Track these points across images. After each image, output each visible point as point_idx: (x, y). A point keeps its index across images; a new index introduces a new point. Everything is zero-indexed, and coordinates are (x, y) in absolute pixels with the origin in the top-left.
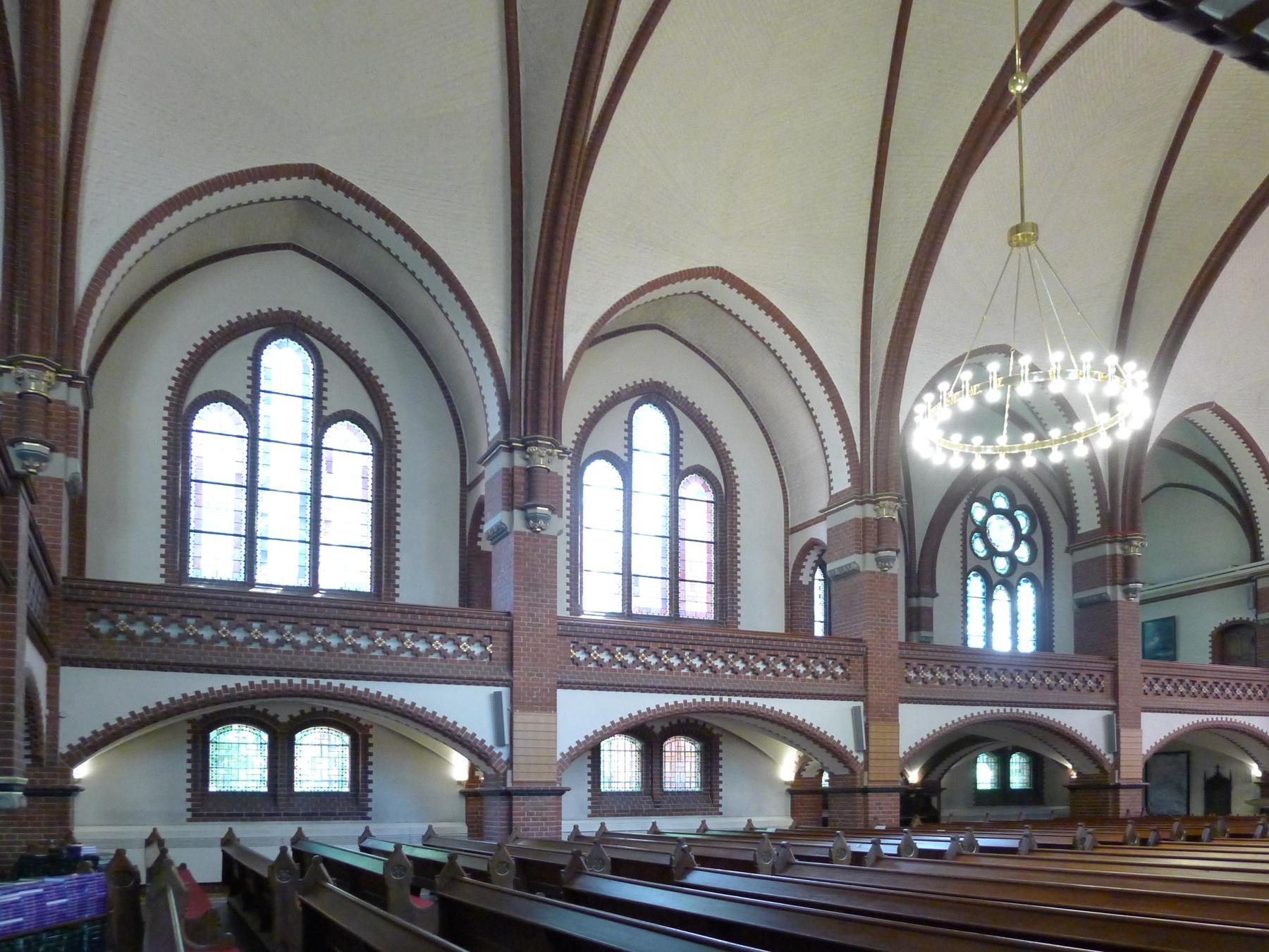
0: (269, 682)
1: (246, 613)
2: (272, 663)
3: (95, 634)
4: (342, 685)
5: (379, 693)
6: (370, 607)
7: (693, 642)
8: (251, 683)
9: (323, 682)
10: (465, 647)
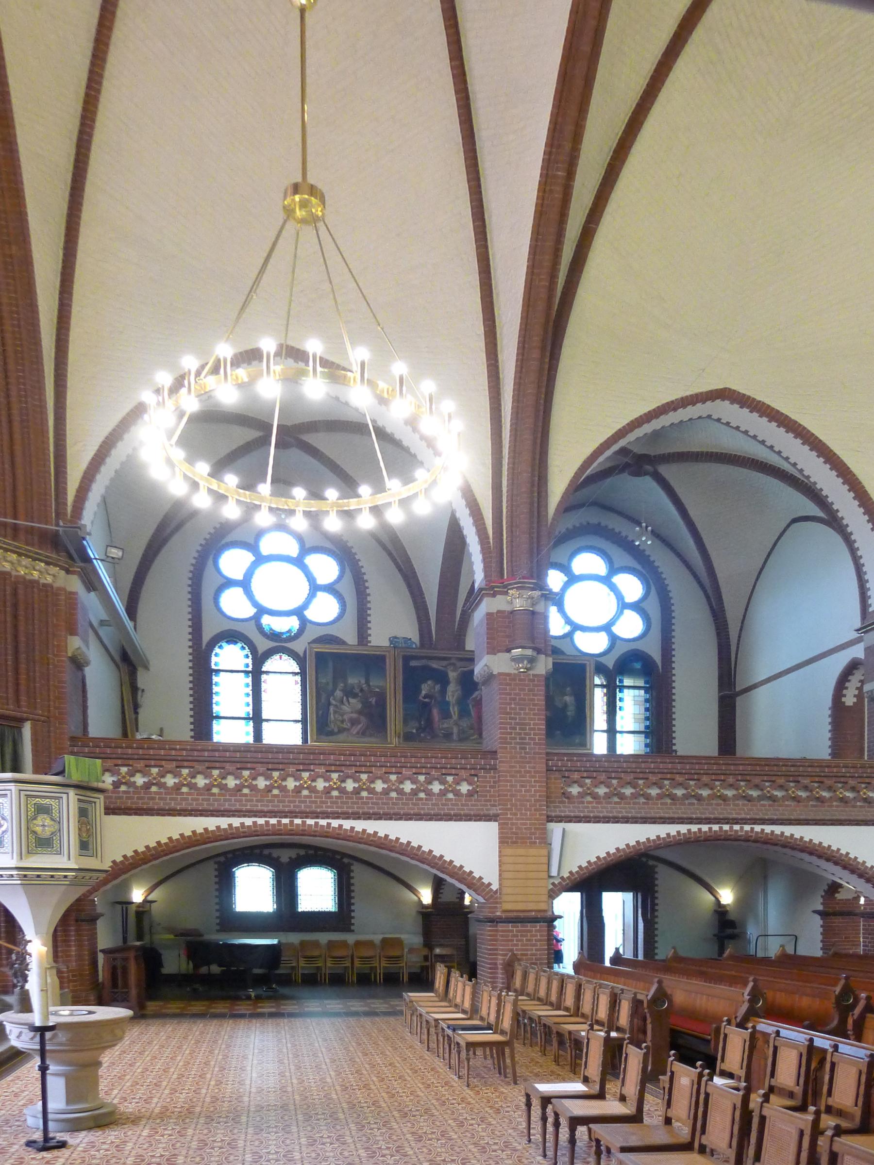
0: (693, 830)
1: (685, 774)
2: (173, 805)
3: (566, 795)
4: (763, 830)
5: (792, 835)
6: (709, 762)
7: (698, 771)
8: (242, 824)
9: (323, 822)
10: (841, 793)
